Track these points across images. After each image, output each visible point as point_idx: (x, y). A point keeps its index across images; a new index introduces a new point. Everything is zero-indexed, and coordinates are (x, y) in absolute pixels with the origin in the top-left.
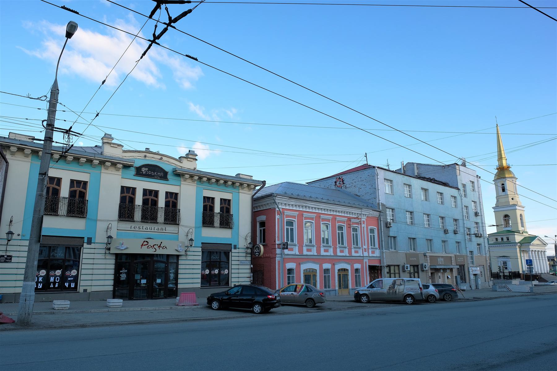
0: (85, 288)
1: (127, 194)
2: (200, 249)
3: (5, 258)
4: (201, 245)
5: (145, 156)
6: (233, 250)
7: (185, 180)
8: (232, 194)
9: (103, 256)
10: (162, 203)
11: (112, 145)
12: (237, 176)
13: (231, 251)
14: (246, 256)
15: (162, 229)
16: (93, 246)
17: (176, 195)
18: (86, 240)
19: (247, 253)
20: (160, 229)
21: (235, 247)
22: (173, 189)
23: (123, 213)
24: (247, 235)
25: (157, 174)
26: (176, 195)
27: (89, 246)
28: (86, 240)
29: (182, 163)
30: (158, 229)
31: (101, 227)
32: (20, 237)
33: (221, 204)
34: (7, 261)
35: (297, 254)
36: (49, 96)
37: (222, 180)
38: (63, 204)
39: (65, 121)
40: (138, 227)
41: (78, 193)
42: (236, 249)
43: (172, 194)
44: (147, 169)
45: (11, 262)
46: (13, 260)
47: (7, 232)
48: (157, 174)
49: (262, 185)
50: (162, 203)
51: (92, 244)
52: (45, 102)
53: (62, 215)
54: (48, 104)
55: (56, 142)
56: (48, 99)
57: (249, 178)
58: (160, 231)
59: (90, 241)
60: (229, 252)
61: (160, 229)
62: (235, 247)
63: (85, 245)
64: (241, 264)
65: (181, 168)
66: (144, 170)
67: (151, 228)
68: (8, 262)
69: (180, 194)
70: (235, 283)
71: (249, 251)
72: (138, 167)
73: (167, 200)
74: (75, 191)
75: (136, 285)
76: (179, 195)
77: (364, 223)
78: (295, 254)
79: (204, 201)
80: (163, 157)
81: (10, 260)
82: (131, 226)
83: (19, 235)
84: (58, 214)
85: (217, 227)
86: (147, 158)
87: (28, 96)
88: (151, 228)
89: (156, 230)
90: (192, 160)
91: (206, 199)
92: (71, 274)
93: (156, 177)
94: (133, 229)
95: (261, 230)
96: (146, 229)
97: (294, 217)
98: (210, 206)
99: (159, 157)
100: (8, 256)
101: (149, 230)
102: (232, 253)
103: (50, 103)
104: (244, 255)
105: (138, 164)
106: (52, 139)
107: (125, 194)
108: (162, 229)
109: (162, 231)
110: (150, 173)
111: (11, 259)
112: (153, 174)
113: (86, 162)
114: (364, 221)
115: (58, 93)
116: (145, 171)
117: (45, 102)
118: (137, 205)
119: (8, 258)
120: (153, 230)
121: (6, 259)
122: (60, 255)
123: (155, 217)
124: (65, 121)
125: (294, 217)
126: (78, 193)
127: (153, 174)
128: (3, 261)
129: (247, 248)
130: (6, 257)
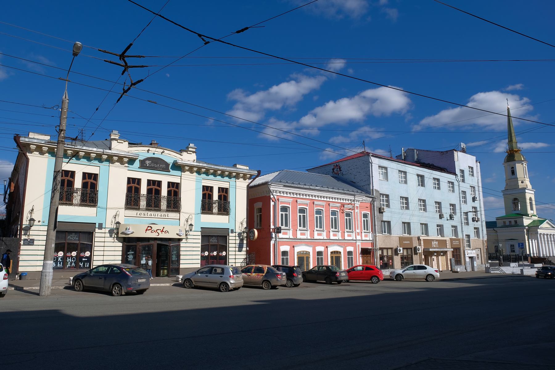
2: (200, 233)
4: (200, 230)
6: (230, 234)
10: (164, 192)
13: (95, 230)
15: (165, 215)
17: (516, 221)
18: (97, 226)
20: (163, 215)
26: (95, 177)
27: (100, 231)
28: (97, 226)
30: (161, 216)
31: (110, 214)
32: (40, 223)
44: (150, 162)
45: (33, 245)
46: (35, 243)
48: (159, 166)
50: (164, 192)
58: (163, 217)
59: (101, 226)
61: (163, 215)
62: (232, 231)
63: (97, 230)
67: (155, 215)
78: (307, 238)
79: (203, 190)
81: (33, 243)
83: (39, 222)
88: (155, 215)
89: (159, 217)
92: (85, 255)
93: (159, 169)
95: (258, 216)
96: (151, 215)
97: (289, 203)
98: (174, 191)
100: (31, 240)
101: (153, 216)
108: (165, 215)
109: (164, 217)
110: (153, 165)
111: (33, 242)
113: (36, 148)
119: (31, 241)
120: (156, 217)
121: (29, 242)
128: (27, 244)
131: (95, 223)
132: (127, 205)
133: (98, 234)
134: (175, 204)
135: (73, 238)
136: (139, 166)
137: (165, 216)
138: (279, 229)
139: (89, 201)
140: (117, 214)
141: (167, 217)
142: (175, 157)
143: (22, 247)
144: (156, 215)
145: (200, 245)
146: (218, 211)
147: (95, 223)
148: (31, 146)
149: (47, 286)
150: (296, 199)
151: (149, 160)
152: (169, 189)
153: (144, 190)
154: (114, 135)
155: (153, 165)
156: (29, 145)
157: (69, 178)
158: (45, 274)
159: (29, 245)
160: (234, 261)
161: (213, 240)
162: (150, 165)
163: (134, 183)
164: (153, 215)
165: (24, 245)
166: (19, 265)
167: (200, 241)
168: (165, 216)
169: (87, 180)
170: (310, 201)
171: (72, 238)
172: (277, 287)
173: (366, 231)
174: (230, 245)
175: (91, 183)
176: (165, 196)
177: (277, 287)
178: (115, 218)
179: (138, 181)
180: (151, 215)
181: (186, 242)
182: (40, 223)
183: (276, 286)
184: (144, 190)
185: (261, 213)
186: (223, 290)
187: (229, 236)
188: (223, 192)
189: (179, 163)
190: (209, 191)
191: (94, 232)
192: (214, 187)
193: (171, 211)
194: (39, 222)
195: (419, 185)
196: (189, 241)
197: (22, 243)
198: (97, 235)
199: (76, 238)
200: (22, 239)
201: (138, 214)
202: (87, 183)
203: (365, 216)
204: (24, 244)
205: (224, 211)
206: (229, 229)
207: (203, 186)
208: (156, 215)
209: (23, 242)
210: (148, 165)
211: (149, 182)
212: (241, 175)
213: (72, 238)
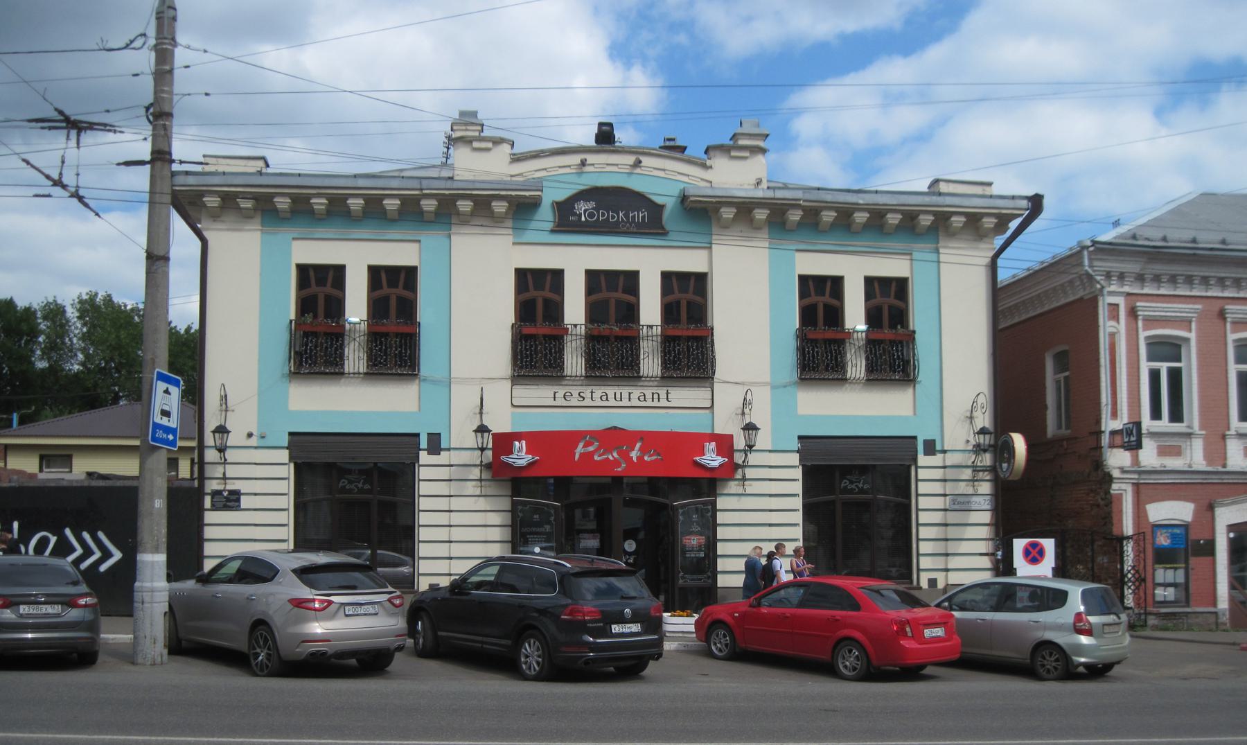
0: (933, 575)
1: (683, 295)
2: (794, 459)
3: (225, 497)
4: (796, 445)
5: (583, 163)
6: (922, 460)
7: (726, 226)
8: (416, 245)
9: (220, 486)
10: (650, 310)
11: (476, 144)
12: (932, 190)
13: (915, 460)
14: (973, 480)
15: (656, 396)
16: (443, 458)
17: (900, 287)
18: (424, 443)
19: (975, 469)
20: (649, 396)
21: (930, 448)
22: (687, 261)
23: (521, 351)
24: (975, 404)
25: (626, 216)
26: (900, 287)
27: (434, 459)
28: (424, 443)
29: (711, 167)
30: (642, 398)
31: (463, 401)
32: (254, 441)
33: (869, 295)
34: (229, 507)
35: (1195, 468)
36: (152, 32)
37: (319, 195)
38: (351, 339)
39: (207, 94)
40: (575, 394)
41: (393, 303)
42: (934, 454)
43: (885, 282)
44: (592, 205)
45: (237, 507)
46: (245, 502)
47: (475, 428)
48: (626, 216)
49: (1027, 212)
50: (650, 310)
51: (442, 453)
52: (145, 51)
53: (574, 374)
54: (153, 54)
55: (181, 162)
56: (152, 42)
57: (978, 190)
58: (649, 403)
59: (435, 445)
60: (909, 467)
61: (649, 396)
62: (930, 448)
63: (424, 457)
64: (956, 507)
65: (709, 185)
66: (582, 207)
67: (618, 396)
68: (233, 507)
69: (420, 267)
70: (434, 580)
71: (987, 459)
72: (662, 211)
73: (808, 301)
74: (606, 302)
75: (681, 574)
76: (709, 276)
77: (1115, 317)
78: (1190, 466)
79: (803, 294)
80: (642, 158)
81: (237, 504)
82: (555, 393)
83: (250, 435)
84: (641, 374)
85: (856, 381)
86: (587, 169)
87: (100, 45)
88: (618, 396)
89: (635, 402)
90: (746, 154)
91: (808, 284)
93: (623, 226)
94: (561, 402)
95: (1058, 382)
96: (604, 398)
97: (1185, 323)
98: (328, 298)
99: (631, 159)
100: (232, 492)
101: (612, 402)
102: (920, 471)
103: (156, 51)
104: (967, 474)
105: (553, 195)
106: (170, 154)
107: (532, 293)
108: (656, 396)
109: (656, 403)
110: (603, 215)
111: (238, 500)
112: (613, 217)
113: (965, 223)
114: (1117, 305)
115: (174, 19)
116: (585, 211)
117: (145, 51)
118: (643, 326)
120: (625, 402)
121: (228, 499)
122: (860, 485)
123: (627, 359)
124: (207, 94)
125: (1185, 323)
126: (393, 303)
127: (613, 217)
128: (221, 505)
129: (979, 449)
130: (225, 494)
131: (417, 435)
132: (872, 371)
133: (428, 469)
134: (688, 350)
135: (356, 486)
136: (550, 226)
137: (656, 400)
138: (1132, 431)
139: (396, 362)
140: (979, 403)
141: (664, 403)
142: (685, 179)
143: (210, 517)
144: (625, 395)
145: (798, 503)
146: (665, 365)
147: (417, 435)
148: (423, 202)
149: (148, 634)
150: (1216, 306)
151: (587, 200)
152: (378, 293)
153: (575, 310)
154: (464, 128)
155: (603, 215)
156: (201, 194)
157: (400, 291)
158: (140, 594)
159: (226, 508)
160: (939, 563)
161: (851, 482)
162: (591, 215)
163: (393, 283)
164: (611, 396)
165: (214, 508)
166: (718, 570)
167: (798, 487)
168: (656, 400)
169: (314, 289)
170: (1199, 306)
171: (853, 486)
172: (929, 670)
173: (1164, 424)
174: (923, 503)
175: (826, 306)
176: (651, 327)
177: (929, 670)
178: (971, 418)
179: (335, 275)
180: (604, 398)
181: (740, 491)
182: (254, 441)
183: (923, 667)
184: (575, 310)
185: (1067, 374)
186: (1049, 671)
187: (917, 468)
188: (885, 294)
189: (692, 199)
190: (878, 295)
191: (416, 465)
192: (845, 277)
193: (677, 377)
194: (250, 435)
195: (147, 109)
196: (752, 488)
197: (208, 502)
198: (423, 473)
199: (364, 484)
200: (208, 490)
201: (560, 394)
202: (386, 299)
203: (1167, 349)
204: (213, 505)
205: (328, 363)
206: (915, 438)
207: (803, 279)
208: (625, 395)
209: (212, 501)
210: (583, 219)
211: (594, 278)
212: (958, 221)
213: (853, 486)
